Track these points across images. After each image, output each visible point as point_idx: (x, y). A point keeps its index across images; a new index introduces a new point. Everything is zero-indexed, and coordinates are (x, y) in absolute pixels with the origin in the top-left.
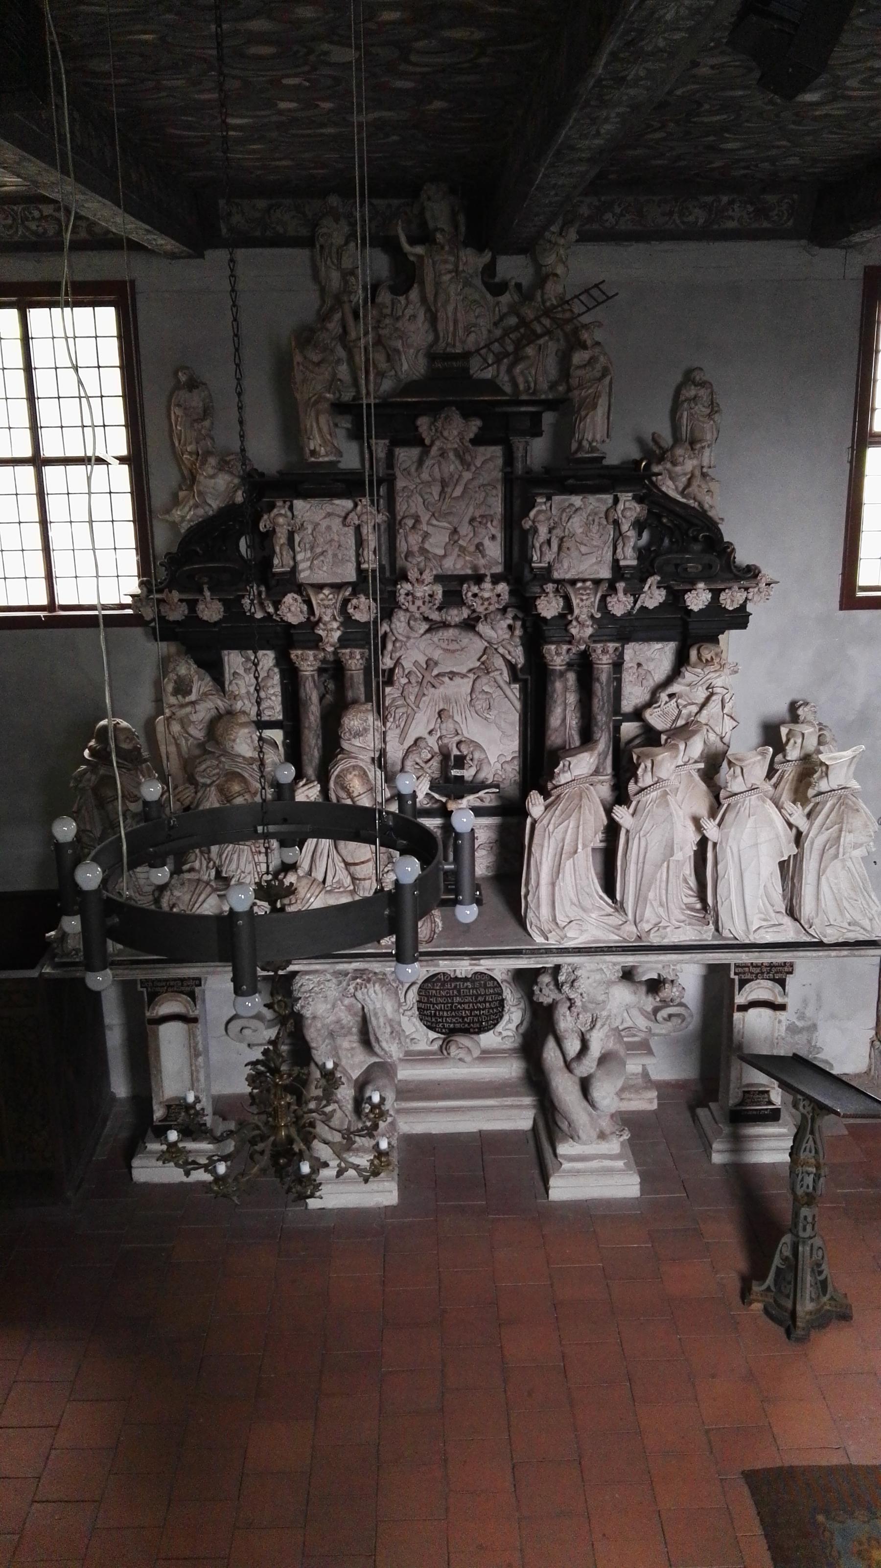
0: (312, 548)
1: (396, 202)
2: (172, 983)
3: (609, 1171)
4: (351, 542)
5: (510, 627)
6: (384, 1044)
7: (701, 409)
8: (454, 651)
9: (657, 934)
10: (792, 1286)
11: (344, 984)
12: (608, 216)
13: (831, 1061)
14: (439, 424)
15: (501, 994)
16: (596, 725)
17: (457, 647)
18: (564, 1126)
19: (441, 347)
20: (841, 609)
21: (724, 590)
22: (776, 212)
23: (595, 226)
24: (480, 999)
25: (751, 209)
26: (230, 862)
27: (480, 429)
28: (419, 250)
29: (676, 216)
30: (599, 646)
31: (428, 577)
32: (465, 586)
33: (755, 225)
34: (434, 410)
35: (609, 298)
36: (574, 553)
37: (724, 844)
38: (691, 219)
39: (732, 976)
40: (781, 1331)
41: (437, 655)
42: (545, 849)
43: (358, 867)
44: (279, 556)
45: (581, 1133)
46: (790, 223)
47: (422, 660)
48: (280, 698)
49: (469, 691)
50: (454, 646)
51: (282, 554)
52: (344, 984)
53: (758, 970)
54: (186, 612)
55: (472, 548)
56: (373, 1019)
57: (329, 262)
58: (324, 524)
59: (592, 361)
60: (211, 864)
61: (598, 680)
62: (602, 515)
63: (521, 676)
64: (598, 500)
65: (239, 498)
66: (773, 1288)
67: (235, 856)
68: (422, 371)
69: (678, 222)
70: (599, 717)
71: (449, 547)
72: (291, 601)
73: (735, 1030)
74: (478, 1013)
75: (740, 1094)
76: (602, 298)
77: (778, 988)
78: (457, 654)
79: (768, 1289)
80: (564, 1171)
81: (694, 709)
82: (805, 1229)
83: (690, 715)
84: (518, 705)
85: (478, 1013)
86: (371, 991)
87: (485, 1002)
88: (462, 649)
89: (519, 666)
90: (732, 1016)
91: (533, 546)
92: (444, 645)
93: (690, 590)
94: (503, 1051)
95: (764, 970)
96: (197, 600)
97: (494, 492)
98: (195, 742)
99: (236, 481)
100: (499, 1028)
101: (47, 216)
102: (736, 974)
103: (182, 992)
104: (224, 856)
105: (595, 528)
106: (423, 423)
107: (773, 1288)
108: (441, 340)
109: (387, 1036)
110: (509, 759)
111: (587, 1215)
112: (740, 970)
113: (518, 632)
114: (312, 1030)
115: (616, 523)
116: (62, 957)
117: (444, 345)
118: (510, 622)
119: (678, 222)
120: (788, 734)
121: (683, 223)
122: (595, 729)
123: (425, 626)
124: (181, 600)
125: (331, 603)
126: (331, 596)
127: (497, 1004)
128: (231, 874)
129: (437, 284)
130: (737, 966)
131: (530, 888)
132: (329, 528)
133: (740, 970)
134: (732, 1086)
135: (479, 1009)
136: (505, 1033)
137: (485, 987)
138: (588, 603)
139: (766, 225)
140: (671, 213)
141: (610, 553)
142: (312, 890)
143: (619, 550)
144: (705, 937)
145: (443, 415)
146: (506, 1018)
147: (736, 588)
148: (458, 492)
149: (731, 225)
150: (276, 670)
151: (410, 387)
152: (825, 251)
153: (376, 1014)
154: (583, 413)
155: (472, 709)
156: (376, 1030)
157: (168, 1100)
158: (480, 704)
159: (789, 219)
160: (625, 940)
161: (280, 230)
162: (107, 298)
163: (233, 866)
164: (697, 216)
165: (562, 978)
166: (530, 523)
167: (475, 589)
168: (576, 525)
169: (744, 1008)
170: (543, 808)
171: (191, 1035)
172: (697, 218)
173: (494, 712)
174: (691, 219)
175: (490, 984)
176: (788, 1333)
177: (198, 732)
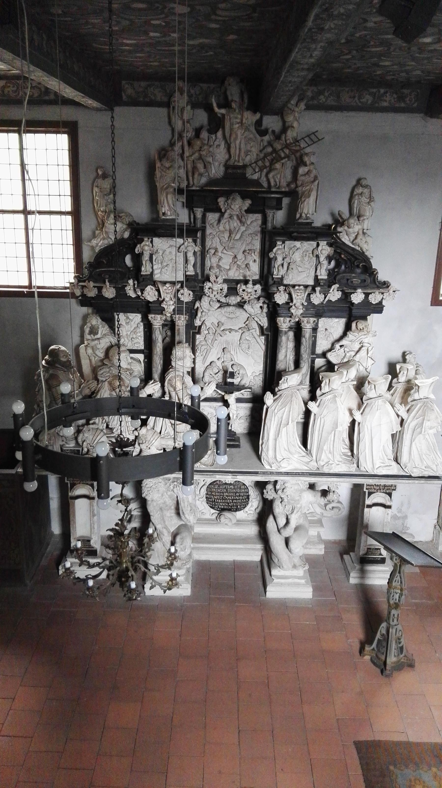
0: (162, 263)
1: (212, 86)
5: (261, 307)
6: (187, 516)
7: (364, 199)
12: (322, 97)
13: (414, 534)
14: (229, 201)
15: (248, 492)
21: (371, 293)
23: (315, 102)
24: (237, 494)
25: (395, 96)
27: (250, 205)
28: (223, 111)
29: (356, 99)
31: (220, 280)
32: (239, 285)
33: (397, 105)
34: (227, 194)
35: (319, 140)
36: (295, 271)
37: (364, 424)
38: (364, 100)
40: (378, 671)
41: (223, 320)
42: (273, 422)
46: (415, 105)
52: (168, 484)
53: (378, 488)
54: (97, 293)
55: (244, 266)
56: (182, 502)
58: (168, 251)
61: (304, 337)
63: (265, 332)
64: (309, 244)
70: (304, 356)
77: (388, 497)
78: (234, 320)
79: (373, 649)
80: (275, 583)
81: (353, 353)
82: (393, 621)
83: (350, 356)
87: (240, 496)
89: (265, 327)
93: (354, 293)
94: (248, 521)
95: (381, 488)
97: (256, 238)
98: (99, 359)
99: (125, 226)
101: (34, 87)
102: (367, 489)
103: (87, 484)
106: (221, 201)
109: (188, 511)
112: (369, 487)
113: (265, 310)
114: (151, 506)
115: (317, 257)
117: (233, 161)
118: (261, 305)
119: (357, 101)
120: (400, 369)
121: (360, 102)
125: (170, 291)
127: (246, 497)
129: (231, 130)
130: (367, 485)
133: (369, 487)
135: (237, 500)
137: (240, 489)
138: (301, 297)
139: (403, 105)
140: (354, 97)
141: (314, 272)
143: (318, 271)
144: (351, 470)
148: (238, 237)
149: (385, 104)
153: (183, 500)
154: (303, 199)
156: (183, 509)
160: (311, 470)
164: (368, 99)
167: (244, 287)
168: (297, 256)
169: (369, 506)
170: (273, 401)
172: (367, 100)
173: (251, 350)
174: (364, 100)
175: (243, 487)
177: (100, 354)
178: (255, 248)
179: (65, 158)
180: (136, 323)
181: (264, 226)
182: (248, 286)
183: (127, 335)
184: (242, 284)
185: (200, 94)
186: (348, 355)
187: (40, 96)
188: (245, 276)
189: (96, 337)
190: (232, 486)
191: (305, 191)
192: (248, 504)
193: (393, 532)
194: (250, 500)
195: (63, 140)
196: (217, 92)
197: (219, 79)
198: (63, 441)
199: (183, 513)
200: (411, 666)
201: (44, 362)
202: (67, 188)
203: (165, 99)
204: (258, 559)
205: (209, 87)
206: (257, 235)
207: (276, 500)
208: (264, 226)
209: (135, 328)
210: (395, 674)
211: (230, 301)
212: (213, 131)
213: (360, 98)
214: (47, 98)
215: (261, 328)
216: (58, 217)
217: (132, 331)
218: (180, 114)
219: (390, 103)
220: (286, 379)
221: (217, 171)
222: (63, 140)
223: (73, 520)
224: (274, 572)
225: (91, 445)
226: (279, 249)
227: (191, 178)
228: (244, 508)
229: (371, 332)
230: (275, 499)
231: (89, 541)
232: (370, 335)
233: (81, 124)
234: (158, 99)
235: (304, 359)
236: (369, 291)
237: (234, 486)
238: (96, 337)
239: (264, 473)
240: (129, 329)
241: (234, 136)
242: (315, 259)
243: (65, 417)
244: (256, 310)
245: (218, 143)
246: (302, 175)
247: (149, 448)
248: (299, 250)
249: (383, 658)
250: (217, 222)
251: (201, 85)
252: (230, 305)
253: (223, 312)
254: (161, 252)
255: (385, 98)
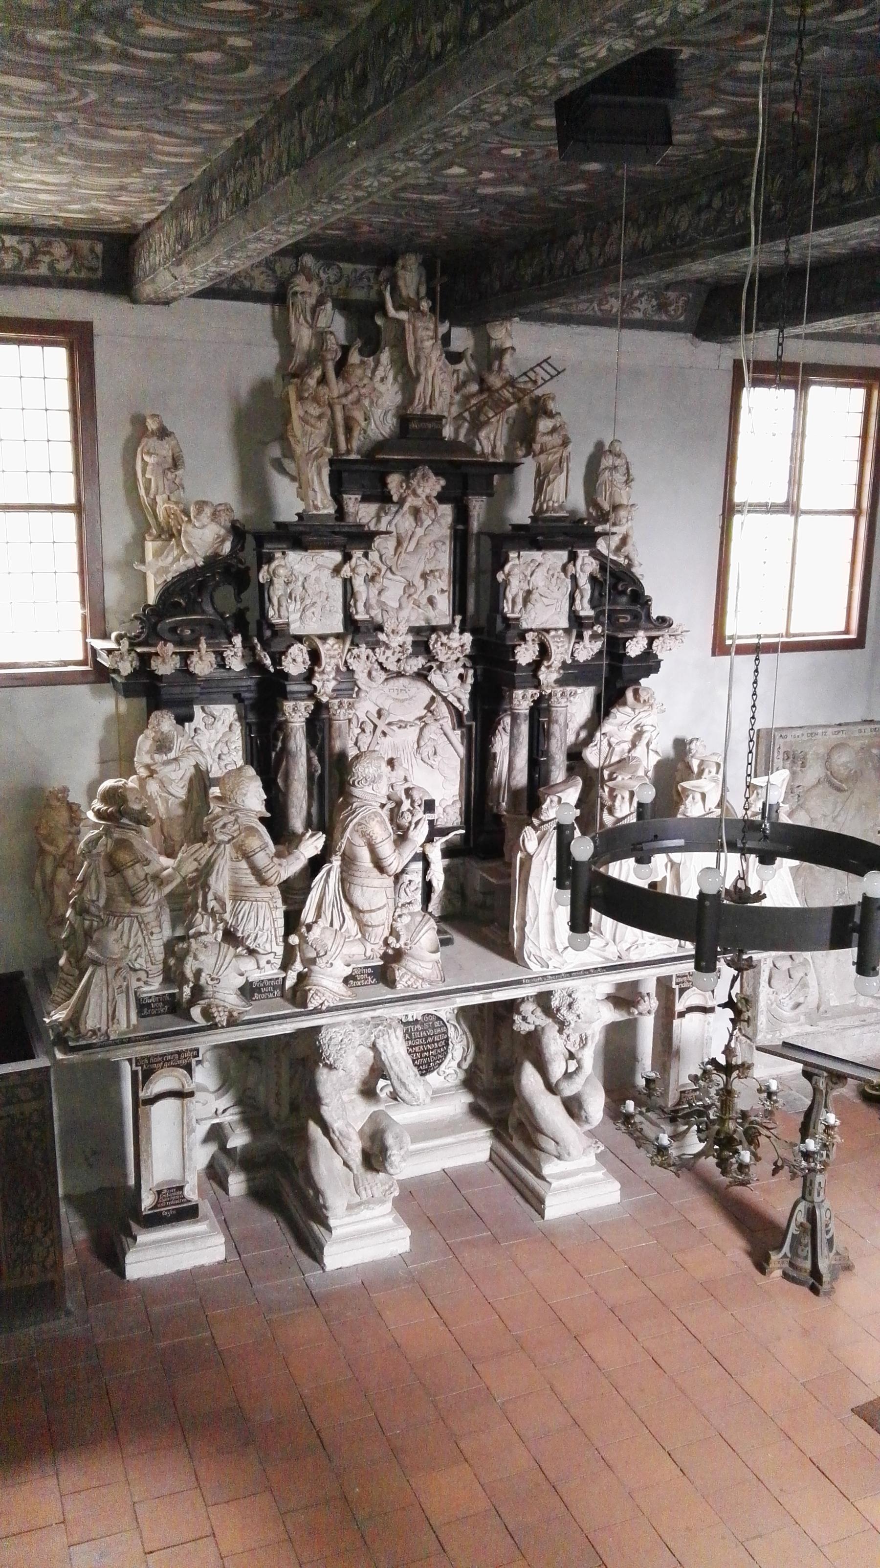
0: (302, 600)
1: (361, 268)
2: (169, 1057)
3: (593, 1182)
4: (339, 592)
5: (461, 677)
6: (412, 1088)
7: (619, 477)
8: (403, 701)
9: (637, 951)
10: (809, 1249)
11: (366, 1033)
14: (414, 482)
15: (446, 1033)
16: (554, 764)
17: (406, 696)
18: (550, 1145)
19: (417, 409)
20: (714, 654)
21: (657, 637)
22: (673, 307)
24: (430, 1040)
25: (654, 302)
26: (248, 920)
27: (443, 487)
28: (403, 315)
30: (336, 701)
31: (403, 628)
32: (434, 636)
33: (656, 318)
34: (408, 469)
35: (559, 373)
36: (539, 605)
37: (688, 864)
38: (606, 307)
39: (674, 986)
40: (806, 1290)
41: (387, 705)
42: (543, 881)
43: (373, 914)
44: (276, 608)
45: (571, 1150)
46: (682, 318)
47: (374, 711)
48: (241, 753)
49: (416, 738)
50: (402, 696)
51: (280, 605)
52: (366, 1033)
54: (178, 666)
55: (424, 601)
56: (393, 1064)
57: (302, 319)
58: (314, 575)
59: (554, 430)
60: (221, 926)
61: (557, 722)
62: (559, 569)
63: (467, 723)
64: (555, 556)
65: (227, 547)
66: (789, 1255)
67: (253, 914)
68: (388, 430)
69: (596, 309)
70: (557, 757)
71: (404, 600)
72: (297, 652)
73: (674, 1036)
74: (427, 1054)
75: (678, 1095)
76: (553, 372)
78: (406, 703)
79: (785, 1256)
80: (555, 1190)
81: (627, 746)
82: (819, 1195)
83: (623, 751)
84: (462, 750)
85: (427, 1054)
86: (393, 1036)
87: (433, 1042)
88: (411, 698)
89: (465, 713)
90: (672, 1023)
91: (505, 597)
92: (394, 695)
93: (631, 638)
94: (449, 1089)
96: (192, 653)
97: (444, 548)
98: (177, 801)
99: (223, 532)
100: (443, 1067)
101: (8, 248)
102: (677, 984)
103: (178, 1066)
104: (240, 916)
105: (554, 580)
106: (394, 481)
107: (789, 1255)
108: (417, 401)
109: (412, 1079)
110: (450, 802)
111: (589, 1227)
112: (680, 980)
113: (470, 680)
114: (328, 1085)
115: (574, 578)
116: (77, 1040)
117: (421, 406)
118: (462, 671)
119: (596, 309)
120: (700, 766)
121: (601, 310)
122: (553, 768)
123: (384, 675)
124: (174, 653)
125: (336, 653)
126: (336, 646)
127: (443, 1043)
128: (246, 934)
129: (418, 349)
130: (678, 977)
131: (527, 919)
132: (317, 580)
133: (680, 980)
134: (671, 1087)
135: (428, 1050)
136: (448, 1072)
137: (434, 1028)
138: (562, 650)
139: (664, 318)
141: (567, 605)
142: (337, 941)
143: (578, 602)
144: (672, 950)
145: (419, 474)
146: (449, 1056)
147: (667, 636)
148: (411, 548)
149: (638, 315)
150: (238, 724)
151: (381, 446)
152: (705, 344)
153: (396, 1060)
154: (551, 476)
155: (418, 756)
156: (401, 1075)
157: (158, 1185)
158: (427, 750)
159: (682, 314)
160: (608, 959)
161: (247, 284)
162: (60, 338)
163: (252, 924)
165: (555, 1003)
166: (503, 576)
167: (444, 639)
168: (539, 580)
169: (682, 1015)
170: (536, 842)
171: (183, 1111)
172: (612, 307)
173: (438, 758)
174: (606, 307)
175: (437, 1024)
176: (815, 1290)
177: (179, 790)
178: (440, 567)
179: (59, 394)
180: (227, 723)
181: (460, 527)
182: (452, 635)
183: (209, 749)
184: (441, 633)
185: (337, 282)
186: (618, 749)
187: (15, 267)
188: (427, 620)
189: (172, 755)
190: (419, 1027)
191: (554, 462)
192: (445, 1056)
193: (723, 1053)
194: (450, 1047)
195: (55, 359)
196: (369, 280)
197: (384, 257)
198: (139, 980)
199: (403, 1084)
200: (848, 1268)
201: (91, 815)
202: (64, 456)
203: (270, 287)
204: (484, 1156)
205: (355, 270)
206: (444, 543)
207: (547, 1029)
208: (460, 527)
209: (224, 735)
210: (835, 1285)
211: (408, 668)
212: (372, 348)
213: (599, 305)
214: (31, 272)
215: (459, 714)
216: (46, 515)
217: (219, 741)
218: (309, 319)
219: (645, 313)
220: (555, 799)
221: (380, 423)
222: (55, 359)
223: (147, 1151)
224: (549, 1169)
225: (214, 976)
226: (514, 565)
227: (342, 438)
228: (440, 1064)
229: (655, 706)
230: (543, 1028)
231: (181, 1188)
232: (655, 710)
233: (98, 328)
234: (257, 287)
235: (558, 763)
236: (654, 633)
237: (422, 1024)
238: (172, 755)
239: (531, 980)
240: (213, 737)
241: (423, 362)
242: (569, 581)
243: (569, 865)
244: (451, 681)
245: (383, 375)
246: (544, 434)
247: (332, 964)
248: (540, 568)
249: (808, 1265)
250: (374, 520)
251: (341, 265)
252: (403, 676)
253: (386, 690)
254: (301, 579)
255: (639, 305)
